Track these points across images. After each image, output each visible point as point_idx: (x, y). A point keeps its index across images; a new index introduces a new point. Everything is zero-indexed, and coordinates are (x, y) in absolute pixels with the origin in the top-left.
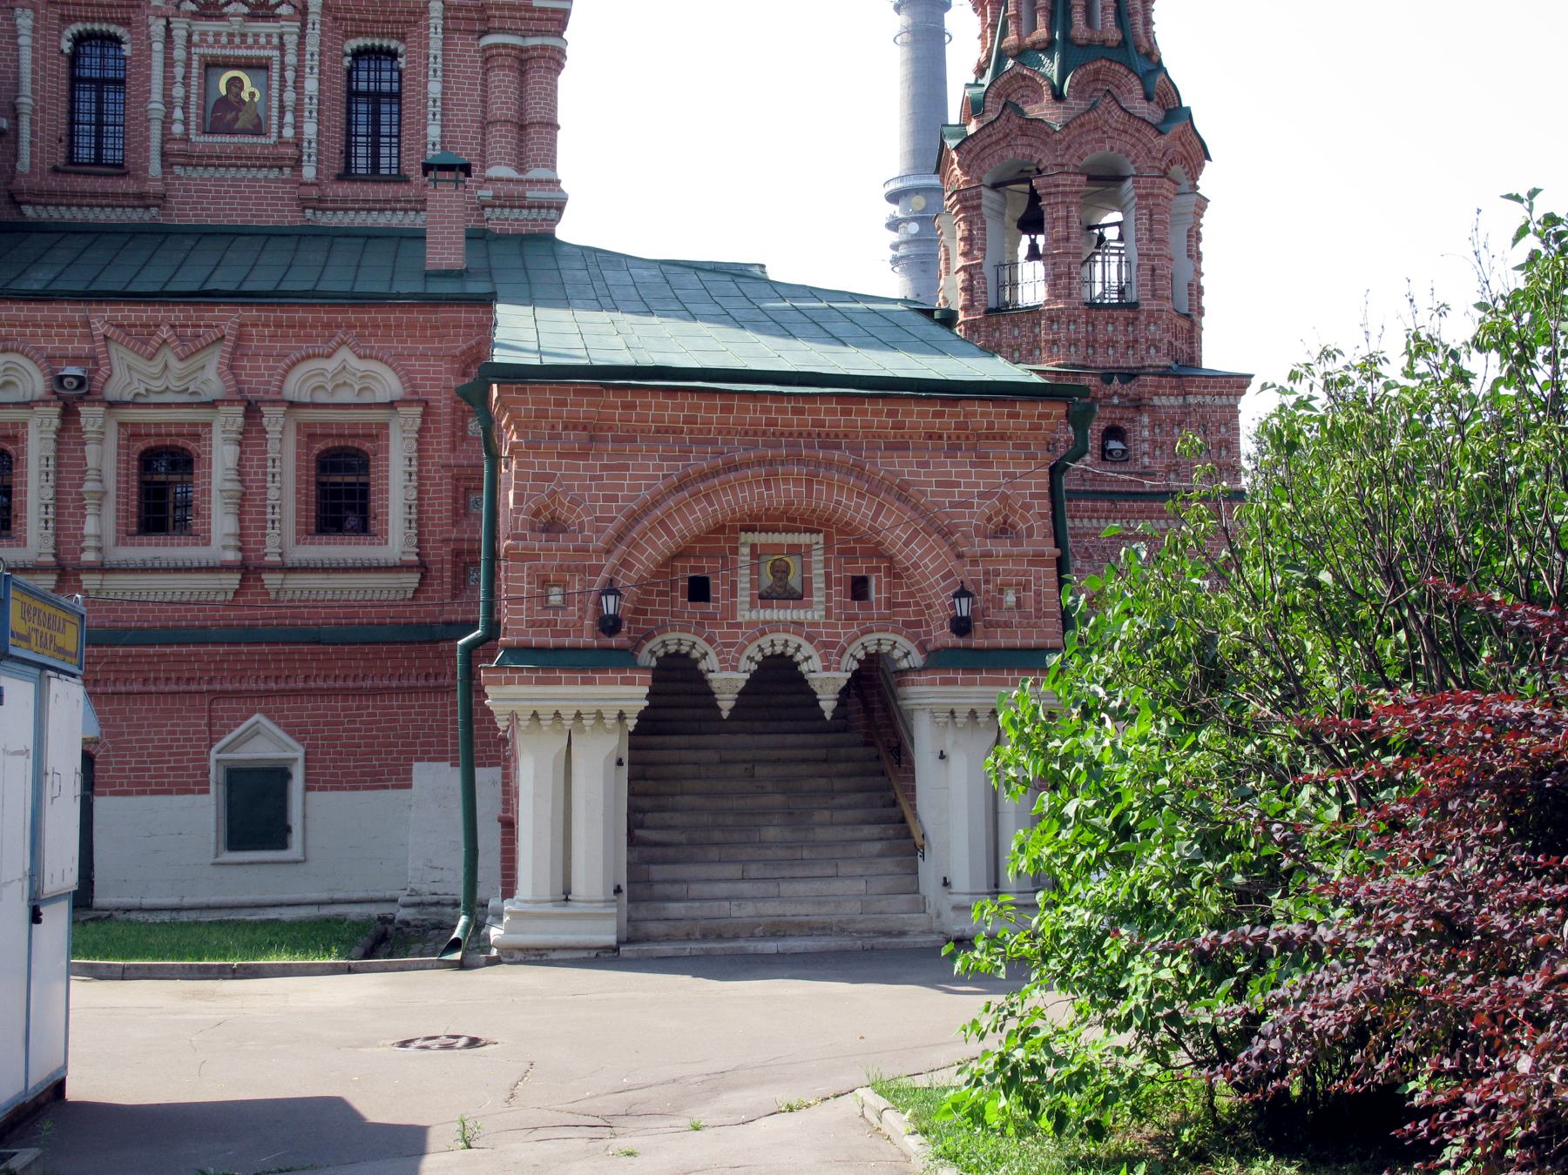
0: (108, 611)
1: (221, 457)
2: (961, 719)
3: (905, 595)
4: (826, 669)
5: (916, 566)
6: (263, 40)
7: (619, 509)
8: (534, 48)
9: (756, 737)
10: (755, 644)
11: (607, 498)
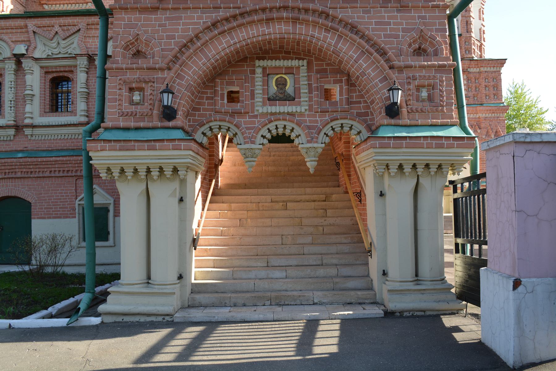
0: (36, 143)
1: (81, 77)
2: (394, 169)
3: (357, 97)
4: (309, 142)
5: (363, 74)
7: (176, 44)
10: (266, 128)
11: (169, 37)
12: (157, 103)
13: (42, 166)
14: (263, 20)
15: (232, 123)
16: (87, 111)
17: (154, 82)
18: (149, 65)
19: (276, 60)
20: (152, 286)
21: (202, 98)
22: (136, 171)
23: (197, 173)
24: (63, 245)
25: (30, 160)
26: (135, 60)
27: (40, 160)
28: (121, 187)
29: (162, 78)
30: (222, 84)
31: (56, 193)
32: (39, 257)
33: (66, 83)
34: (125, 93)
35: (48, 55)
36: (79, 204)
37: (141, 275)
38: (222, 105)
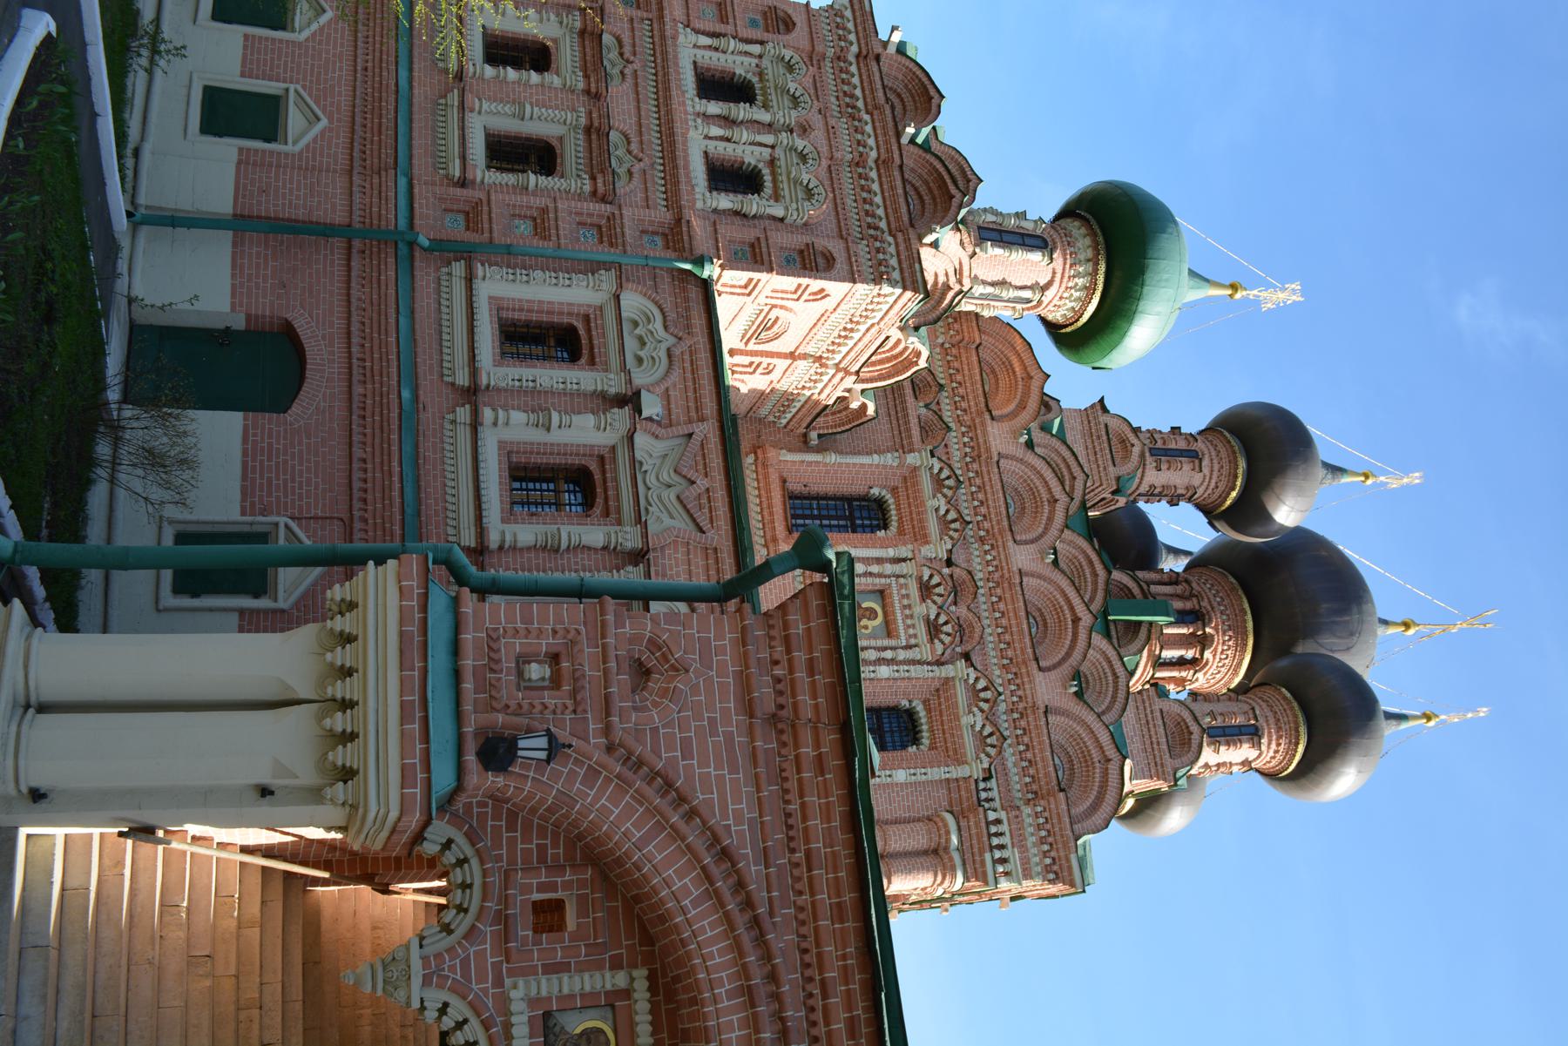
1: (594, 534)
6: (911, 631)
7: (672, 762)
8: (951, 859)
9: (300, 967)
10: (469, 1014)
12: (523, 721)
13: (377, 441)
14: (748, 978)
15: (478, 918)
16: (514, 548)
17: (574, 711)
18: (616, 698)
19: (651, 1023)
20: (17, 718)
21: (542, 832)
22: (346, 672)
23: (339, 829)
24: (167, 485)
25: (395, 414)
26: (625, 666)
27: (395, 437)
28: (306, 635)
29: (586, 731)
30: (582, 884)
31: (308, 470)
32: (138, 426)
33: (580, 500)
34: (545, 644)
35: (641, 463)
36: (277, 524)
37: (50, 684)
38: (526, 889)
